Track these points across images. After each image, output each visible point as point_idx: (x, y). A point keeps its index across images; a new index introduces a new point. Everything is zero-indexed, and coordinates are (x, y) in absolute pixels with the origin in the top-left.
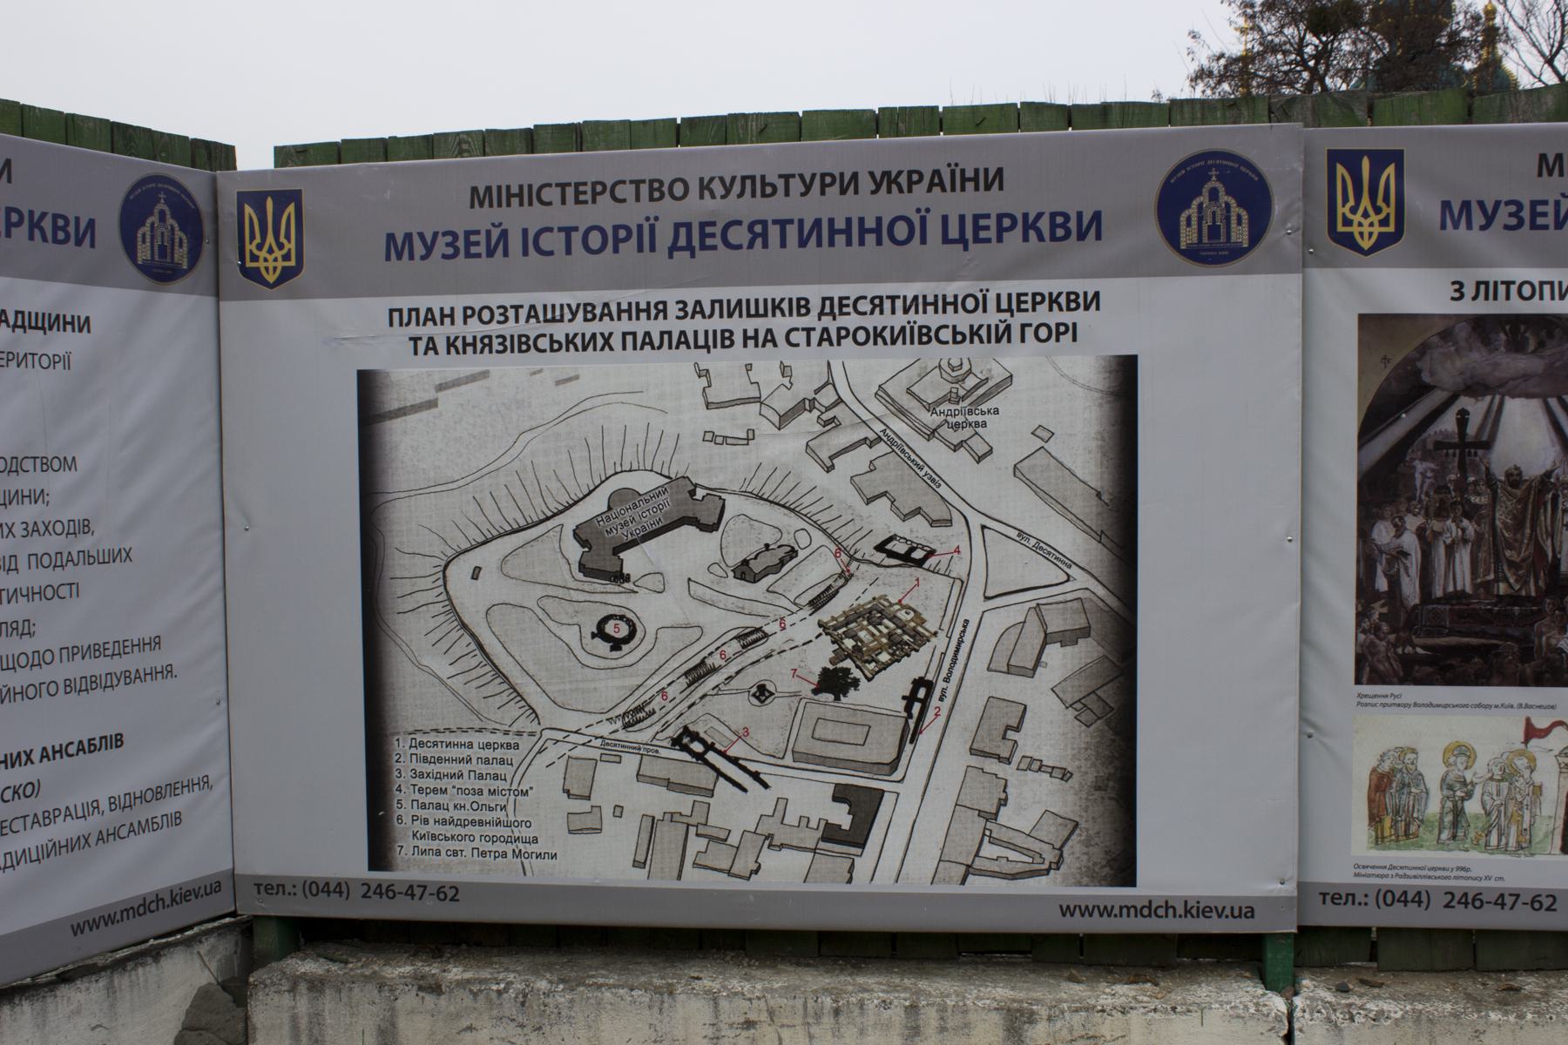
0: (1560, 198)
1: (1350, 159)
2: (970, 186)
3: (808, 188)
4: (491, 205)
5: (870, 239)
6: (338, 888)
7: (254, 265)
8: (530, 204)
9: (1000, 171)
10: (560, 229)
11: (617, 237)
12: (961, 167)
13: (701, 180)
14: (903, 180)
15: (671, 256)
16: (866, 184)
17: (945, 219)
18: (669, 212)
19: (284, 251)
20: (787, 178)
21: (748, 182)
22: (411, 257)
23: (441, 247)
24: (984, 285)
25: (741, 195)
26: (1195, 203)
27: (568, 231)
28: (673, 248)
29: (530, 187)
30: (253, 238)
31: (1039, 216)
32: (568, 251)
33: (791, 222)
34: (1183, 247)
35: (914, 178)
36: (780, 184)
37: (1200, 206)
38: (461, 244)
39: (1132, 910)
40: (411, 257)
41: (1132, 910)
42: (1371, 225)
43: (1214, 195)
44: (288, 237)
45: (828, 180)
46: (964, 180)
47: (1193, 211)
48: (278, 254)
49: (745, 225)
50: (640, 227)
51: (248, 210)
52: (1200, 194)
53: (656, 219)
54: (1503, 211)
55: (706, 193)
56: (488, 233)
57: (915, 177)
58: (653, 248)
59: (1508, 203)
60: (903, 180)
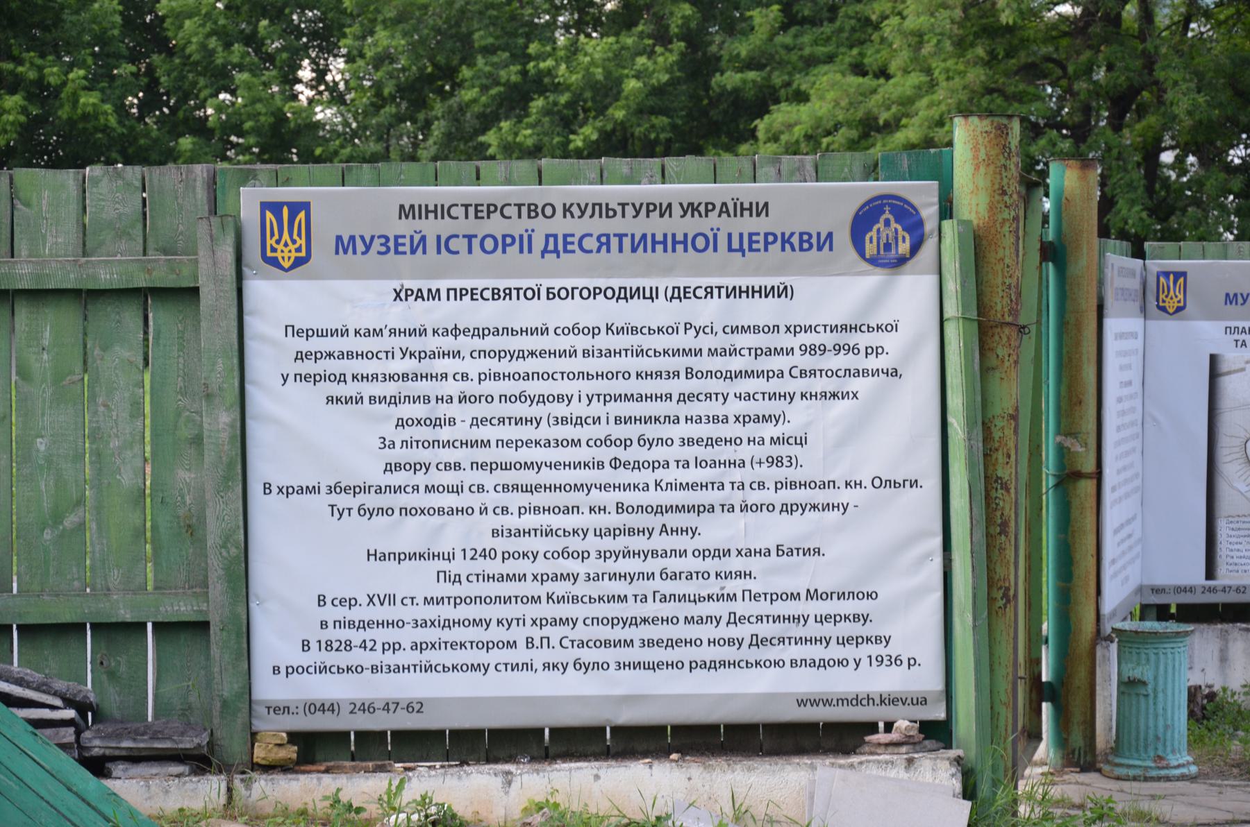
0: (413, 233)
1: (275, 208)
2: (746, 213)
3: (638, 213)
4: (414, 218)
5: (680, 247)
6: (1190, 589)
7: (274, 255)
8: (443, 217)
9: (766, 205)
10: (464, 236)
11: (505, 242)
12: (741, 200)
13: (565, 205)
14: (702, 209)
15: (543, 257)
16: (677, 211)
17: (730, 235)
18: (541, 226)
19: (297, 246)
20: (623, 205)
21: (597, 208)
22: (355, 252)
23: (377, 246)
24: (539, 281)
25: (592, 216)
26: (875, 228)
27: (470, 238)
28: (545, 251)
29: (443, 206)
30: (272, 235)
31: (792, 234)
32: (470, 251)
33: (626, 235)
34: (867, 256)
35: (709, 207)
36: (619, 209)
37: (878, 230)
38: (391, 244)
39: (845, 702)
40: (355, 252)
41: (845, 702)
42: (290, 251)
43: (887, 223)
44: (299, 235)
45: (651, 207)
46: (742, 209)
47: (873, 233)
48: (292, 247)
49: (595, 236)
50: (521, 237)
51: (269, 215)
52: (878, 222)
53: (533, 231)
54: (377, 242)
55: (568, 214)
56: (412, 237)
57: (710, 207)
58: (530, 251)
59: (379, 237)
60: (702, 209)
